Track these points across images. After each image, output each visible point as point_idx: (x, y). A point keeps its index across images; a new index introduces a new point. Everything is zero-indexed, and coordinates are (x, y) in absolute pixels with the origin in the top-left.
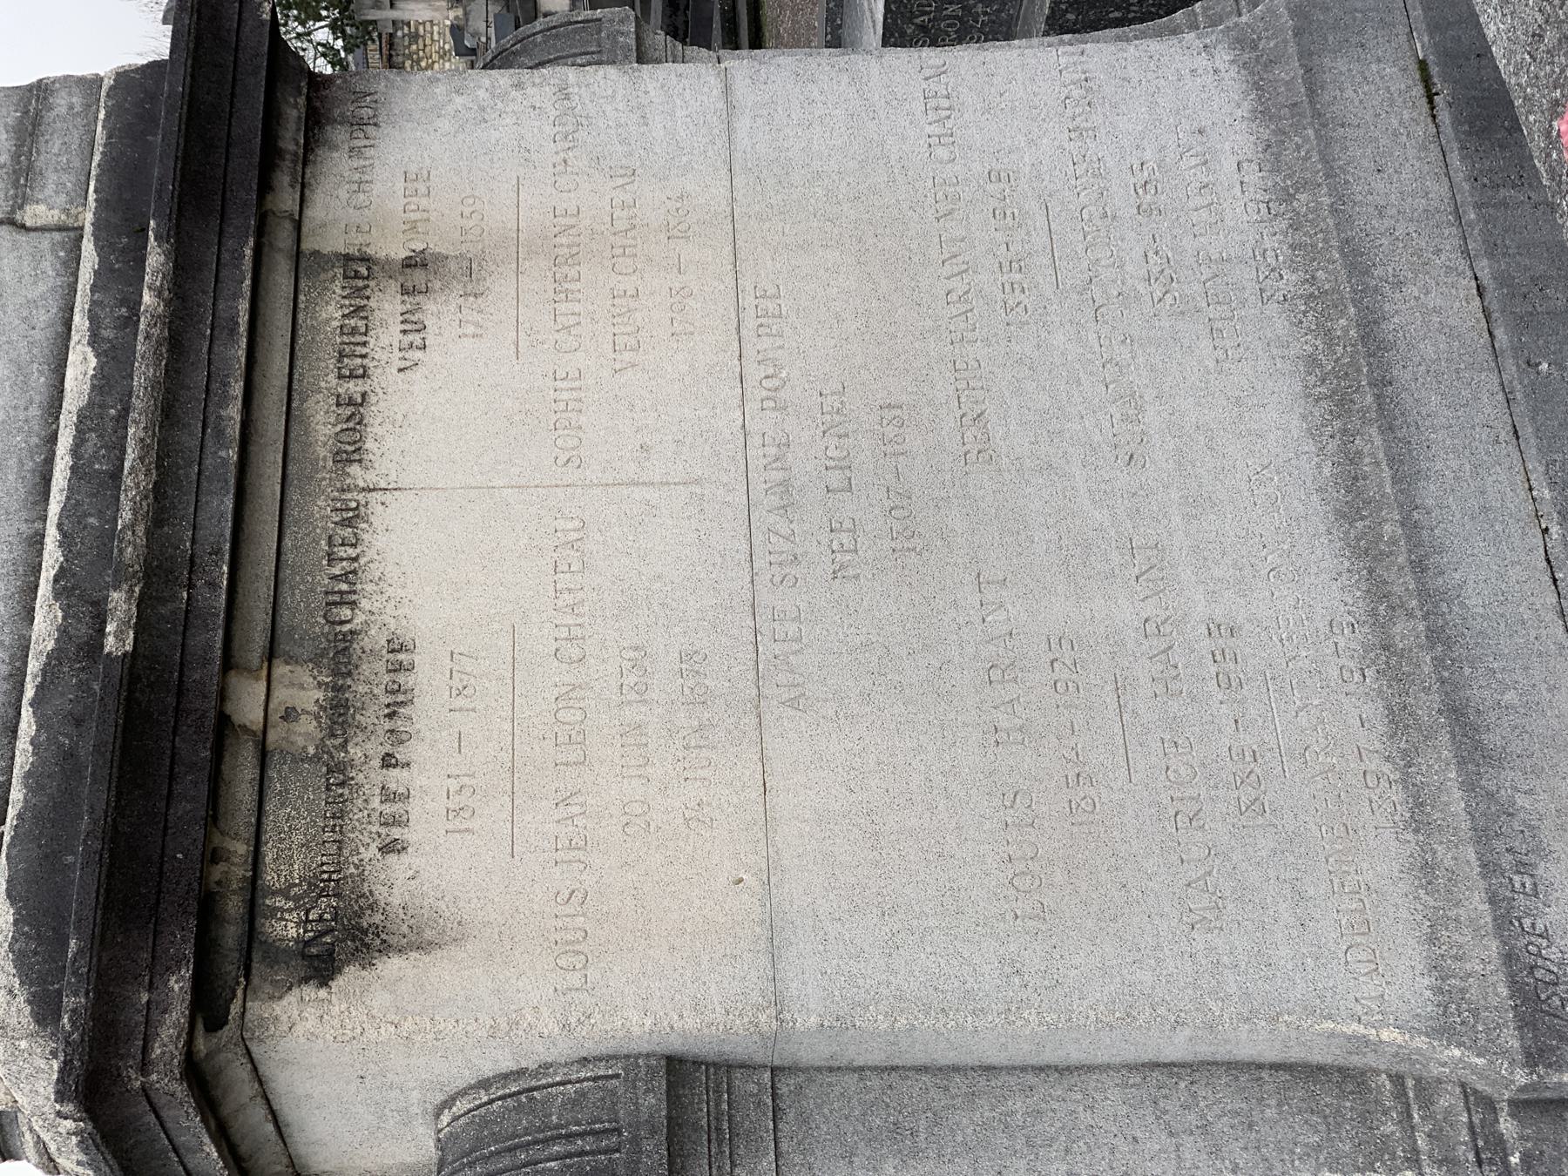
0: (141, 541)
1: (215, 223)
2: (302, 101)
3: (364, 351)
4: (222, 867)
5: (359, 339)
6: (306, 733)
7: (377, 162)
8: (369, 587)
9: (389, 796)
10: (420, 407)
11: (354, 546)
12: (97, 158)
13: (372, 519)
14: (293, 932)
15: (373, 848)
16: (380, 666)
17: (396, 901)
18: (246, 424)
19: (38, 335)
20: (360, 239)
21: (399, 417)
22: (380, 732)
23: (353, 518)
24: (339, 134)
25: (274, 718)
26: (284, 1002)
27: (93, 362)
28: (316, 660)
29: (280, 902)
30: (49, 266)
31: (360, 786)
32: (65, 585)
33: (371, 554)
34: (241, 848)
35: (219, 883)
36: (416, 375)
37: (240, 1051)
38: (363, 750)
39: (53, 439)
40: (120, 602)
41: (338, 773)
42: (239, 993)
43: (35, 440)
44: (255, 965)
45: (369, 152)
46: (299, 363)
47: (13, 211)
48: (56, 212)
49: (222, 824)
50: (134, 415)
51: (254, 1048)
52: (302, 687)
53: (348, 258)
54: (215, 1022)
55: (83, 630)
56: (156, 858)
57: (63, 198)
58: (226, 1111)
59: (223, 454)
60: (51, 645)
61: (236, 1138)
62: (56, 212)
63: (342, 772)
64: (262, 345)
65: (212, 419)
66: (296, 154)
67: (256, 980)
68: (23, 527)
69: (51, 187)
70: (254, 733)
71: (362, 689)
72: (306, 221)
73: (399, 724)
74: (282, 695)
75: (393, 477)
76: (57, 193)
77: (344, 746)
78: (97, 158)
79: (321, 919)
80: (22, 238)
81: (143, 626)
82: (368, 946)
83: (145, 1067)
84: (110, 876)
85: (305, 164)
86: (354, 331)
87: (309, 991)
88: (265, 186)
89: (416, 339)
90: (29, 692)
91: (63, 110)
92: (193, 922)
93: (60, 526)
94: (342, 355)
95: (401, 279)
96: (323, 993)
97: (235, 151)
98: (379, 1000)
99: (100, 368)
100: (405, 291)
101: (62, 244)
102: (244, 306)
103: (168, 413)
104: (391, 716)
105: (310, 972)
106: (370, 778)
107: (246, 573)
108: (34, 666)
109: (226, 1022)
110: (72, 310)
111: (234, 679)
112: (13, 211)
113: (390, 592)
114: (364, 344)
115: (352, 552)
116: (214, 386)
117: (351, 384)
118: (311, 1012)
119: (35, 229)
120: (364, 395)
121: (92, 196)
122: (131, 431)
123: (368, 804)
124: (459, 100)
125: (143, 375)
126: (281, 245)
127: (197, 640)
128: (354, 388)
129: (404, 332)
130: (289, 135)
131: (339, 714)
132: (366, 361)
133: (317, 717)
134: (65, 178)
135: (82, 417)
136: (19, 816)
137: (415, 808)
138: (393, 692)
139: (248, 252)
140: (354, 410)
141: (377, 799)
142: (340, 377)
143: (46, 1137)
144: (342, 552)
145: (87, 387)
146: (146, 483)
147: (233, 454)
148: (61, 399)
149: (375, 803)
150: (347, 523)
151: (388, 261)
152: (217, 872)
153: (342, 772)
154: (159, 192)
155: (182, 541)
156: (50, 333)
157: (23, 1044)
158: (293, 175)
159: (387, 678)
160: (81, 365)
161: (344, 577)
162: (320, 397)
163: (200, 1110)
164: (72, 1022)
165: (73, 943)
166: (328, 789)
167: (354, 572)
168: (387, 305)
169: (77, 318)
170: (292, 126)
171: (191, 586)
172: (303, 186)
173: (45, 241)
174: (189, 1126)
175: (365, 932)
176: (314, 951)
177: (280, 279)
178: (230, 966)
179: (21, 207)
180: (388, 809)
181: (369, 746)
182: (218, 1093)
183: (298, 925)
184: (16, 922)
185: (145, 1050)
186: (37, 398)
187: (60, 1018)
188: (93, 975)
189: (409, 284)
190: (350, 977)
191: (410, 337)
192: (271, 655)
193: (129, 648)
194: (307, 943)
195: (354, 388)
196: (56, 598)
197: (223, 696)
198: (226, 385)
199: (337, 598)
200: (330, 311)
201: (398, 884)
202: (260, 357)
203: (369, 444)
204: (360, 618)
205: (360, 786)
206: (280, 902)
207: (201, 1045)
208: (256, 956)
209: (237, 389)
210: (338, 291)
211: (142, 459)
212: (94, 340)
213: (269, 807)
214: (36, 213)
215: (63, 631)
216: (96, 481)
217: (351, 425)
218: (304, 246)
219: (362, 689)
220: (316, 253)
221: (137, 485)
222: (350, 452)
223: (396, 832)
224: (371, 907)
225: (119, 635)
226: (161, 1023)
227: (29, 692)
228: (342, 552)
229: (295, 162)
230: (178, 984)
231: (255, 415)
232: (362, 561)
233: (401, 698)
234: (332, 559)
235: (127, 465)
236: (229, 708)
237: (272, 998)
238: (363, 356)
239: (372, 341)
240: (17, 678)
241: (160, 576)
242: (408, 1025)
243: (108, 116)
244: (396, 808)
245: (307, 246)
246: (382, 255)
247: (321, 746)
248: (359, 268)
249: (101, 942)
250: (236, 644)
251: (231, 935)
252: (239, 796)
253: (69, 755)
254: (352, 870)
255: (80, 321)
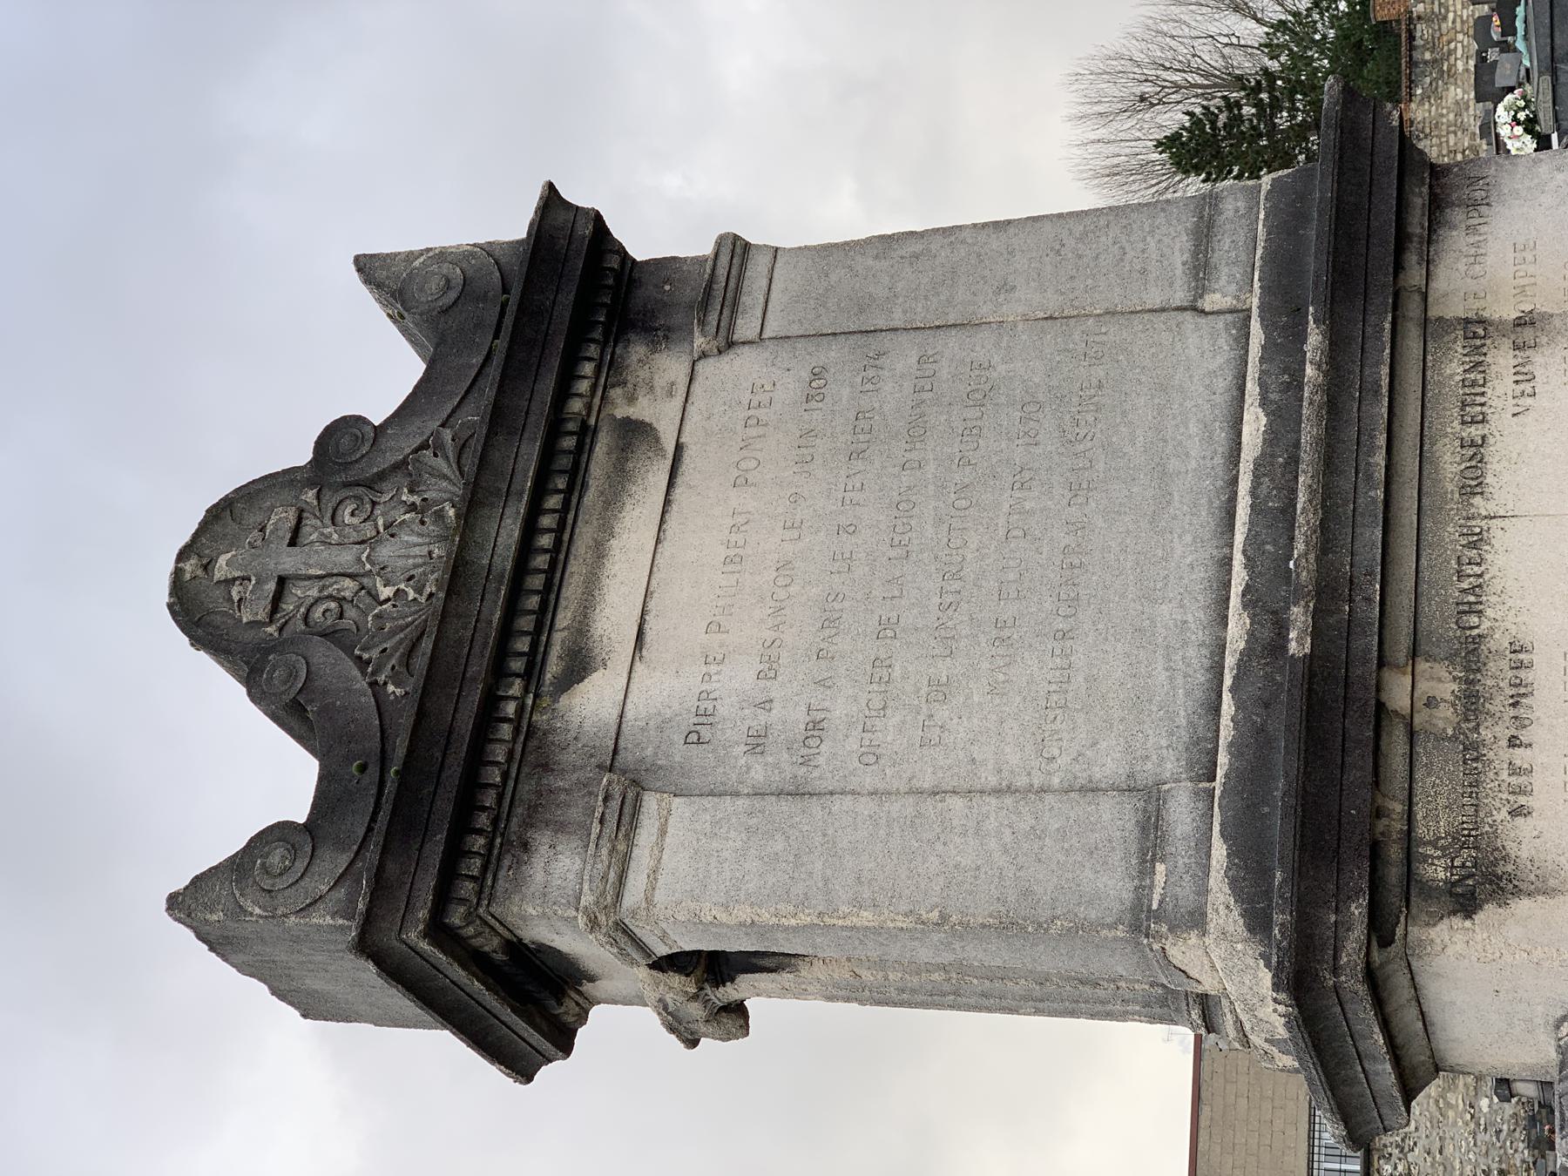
0: (1313, 567)
1: (1360, 303)
2: (1425, 190)
3: (1483, 400)
4: (1384, 821)
5: (1478, 390)
6: (1445, 717)
7: (1489, 237)
8: (1493, 599)
9: (1515, 771)
10: (1531, 447)
11: (1479, 564)
12: (1259, 252)
13: (1493, 541)
14: (1441, 875)
15: (1504, 814)
16: (1504, 664)
17: (1524, 854)
18: (1388, 467)
19: (1218, 399)
20: (1478, 304)
21: (1514, 455)
22: (1506, 718)
23: (1477, 541)
24: (1457, 215)
25: (1419, 705)
26: (1438, 928)
27: (1264, 420)
28: (1451, 658)
29: (1430, 851)
30: (1224, 342)
31: (1491, 762)
32: (1251, 598)
33: (1493, 571)
34: (1398, 808)
35: (1382, 834)
36: (1528, 419)
37: (1404, 964)
38: (1493, 732)
39: (1234, 481)
40: (1299, 615)
41: (1472, 751)
42: (1402, 919)
43: (1220, 483)
44: (1413, 899)
45: (1483, 229)
46: (1428, 413)
47: (1195, 300)
48: (1229, 299)
49: (1382, 788)
50: (1303, 466)
51: (1414, 964)
52: (1440, 680)
53: (1467, 321)
54: (1386, 942)
55: (1266, 634)
56: (1335, 813)
57: (1233, 287)
58: (1389, 1009)
59: (1372, 494)
60: (1242, 645)
61: (1395, 1032)
62: (1229, 299)
63: (1476, 749)
64: (1399, 399)
65: (1362, 467)
66: (1421, 237)
67: (1414, 911)
68: (1215, 552)
69: (1224, 278)
70: (1404, 717)
71: (1490, 682)
72: (1431, 292)
73: (1521, 711)
74: (1424, 687)
75: (1510, 506)
76: (1229, 283)
77: (1476, 729)
78: (1259, 252)
79: (1463, 866)
80: (1202, 320)
81: (1316, 634)
82: (1502, 889)
83: (1336, 971)
84: (1303, 824)
85: (1429, 243)
86: (1474, 384)
87: (1457, 921)
88: (1399, 267)
89: (1527, 387)
90: (1228, 681)
91: (1230, 214)
92: (1367, 864)
93: (1244, 552)
94: (1464, 405)
95: (1513, 337)
96: (1468, 923)
97: (1374, 240)
98: (1514, 932)
99: (1270, 425)
100: (1516, 347)
101: (1234, 323)
102: (1385, 371)
103: (1329, 463)
104: (1514, 705)
105: (1457, 907)
106: (1500, 755)
107: (1393, 588)
108: (1230, 661)
109: (1393, 941)
110: (1244, 377)
111: (1387, 674)
112: (1195, 300)
113: (1510, 603)
114: (1483, 394)
115: (1477, 570)
116: (1363, 438)
117: (1472, 429)
118: (1459, 937)
119: (1212, 313)
120: (1483, 437)
121: (1257, 284)
122: (1301, 479)
123: (1498, 777)
124: (1560, 177)
125: (1308, 434)
126: (1411, 314)
127: (1358, 644)
128: (1475, 432)
129: (1517, 382)
130: (1416, 221)
131: (1472, 702)
132: (1484, 409)
133: (1454, 705)
134: (1235, 270)
135: (1258, 464)
136: (1226, 776)
137: (1537, 780)
138: (1515, 686)
139: (1387, 326)
140: (1476, 451)
141: (1506, 773)
142: (1463, 423)
143: (1243, 1017)
144: (1469, 570)
145: (1260, 441)
146: (1315, 521)
147: (1380, 494)
148: (1239, 450)
149: (1504, 775)
150: (1473, 545)
151: (1501, 322)
152: (1381, 825)
153: (1476, 749)
154: (1316, 284)
155: (1343, 565)
156: (1227, 397)
157: (1239, 947)
158: (1420, 255)
159: (1510, 674)
160: (1255, 423)
161: (1472, 590)
162: (1447, 440)
163: (1373, 1005)
164: (1282, 934)
165: (1278, 874)
166: (1465, 763)
167: (1480, 586)
168: (1502, 360)
169: (1249, 385)
170: (1418, 212)
171: (1351, 601)
172: (1428, 262)
173: (1220, 322)
174: (1364, 1016)
175: (1500, 878)
176: (1459, 890)
177: (1412, 344)
178: (1394, 898)
179: (1201, 296)
180: (1514, 780)
181: (1497, 729)
182: (1385, 995)
183: (1446, 869)
184: (1229, 856)
185: (1336, 958)
186: (1220, 450)
187: (1271, 929)
188: (1295, 900)
189: (1520, 341)
190: (1488, 913)
191: (1522, 386)
192: (1414, 654)
193: (1307, 651)
194: (1454, 884)
195: (1475, 432)
196: (1245, 607)
197: (1378, 689)
198: (1372, 437)
199: (1466, 608)
200: (1454, 368)
201: (1526, 841)
202: (1397, 411)
203: (1489, 479)
204: (1486, 624)
205: (1491, 762)
206: (1430, 851)
207: (1376, 957)
208: (1413, 892)
209: (1382, 440)
210: (1460, 350)
211: (1310, 501)
212: (1264, 402)
213: (1418, 776)
214: (1212, 301)
215: (1251, 635)
216: (1275, 517)
217: (1473, 463)
218: (1430, 314)
219: (1490, 682)
220: (1440, 319)
221: (1308, 523)
222: (1473, 486)
223: (1522, 800)
224: (1504, 858)
225: (1299, 640)
226: (1346, 938)
227: (1228, 681)
228: (1469, 570)
229: (1421, 243)
230: (1358, 910)
231: (1396, 459)
232: (1487, 577)
233: (1522, 690)
234: (1461, 576)
235: (1299, 506)
236: (1384, 697)
237: (1428, 925)
238: (1482, 405)
239: (1489, 392)
240: (1217, 670)
241: (1329, 593)
242: (1538, 954)
243: (1267, 216)
244: (1522, 780)
245: (1433, 313)
246: (1496, 316)
247: (1458, 727)
248: (1476, 330)
249: (1298, 874)
250: (1386, 646)
251: (1394, 874)
252: (1394, 766)
253: (1261, 730)
254: (1487, 828)
255: (1252, 388)
